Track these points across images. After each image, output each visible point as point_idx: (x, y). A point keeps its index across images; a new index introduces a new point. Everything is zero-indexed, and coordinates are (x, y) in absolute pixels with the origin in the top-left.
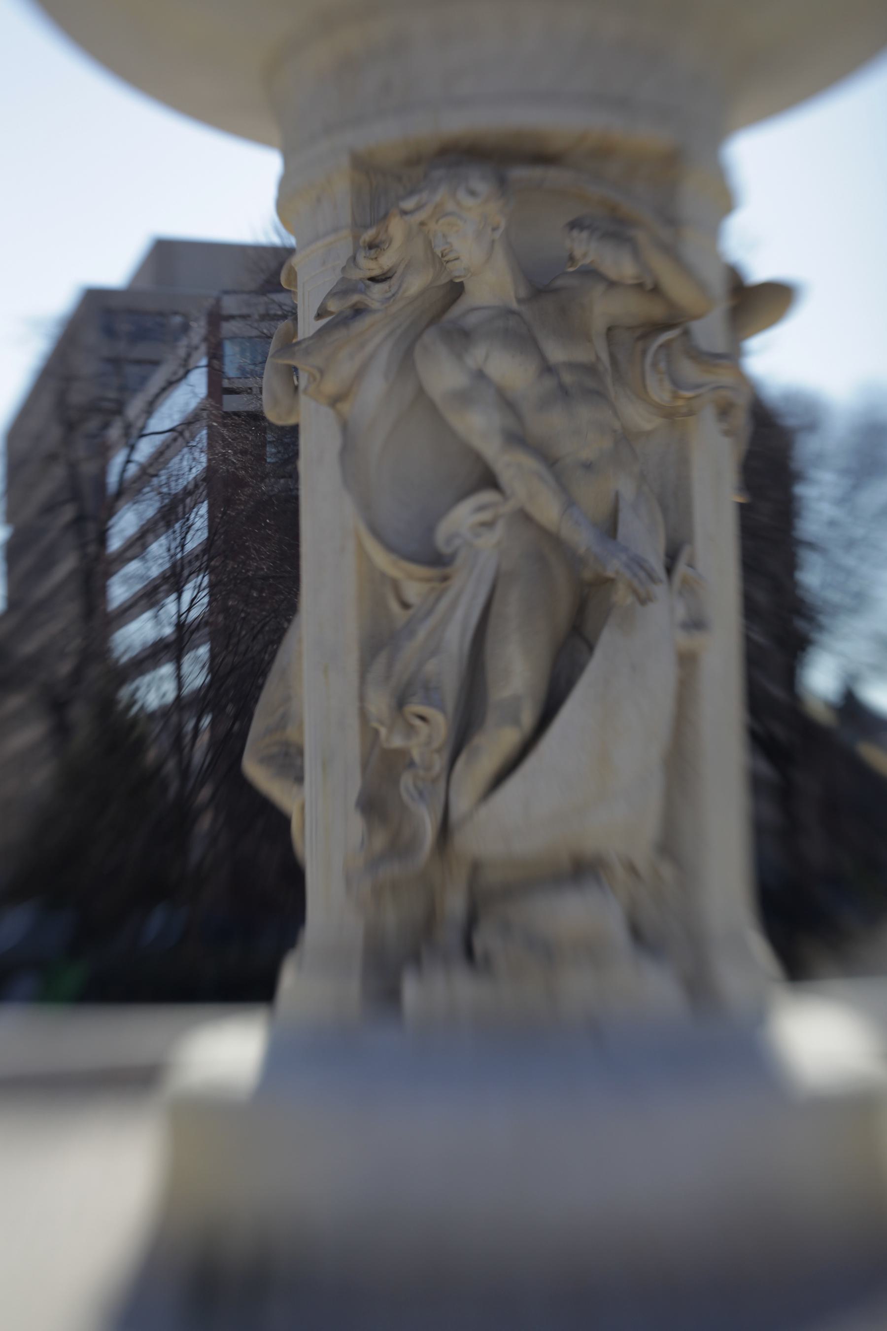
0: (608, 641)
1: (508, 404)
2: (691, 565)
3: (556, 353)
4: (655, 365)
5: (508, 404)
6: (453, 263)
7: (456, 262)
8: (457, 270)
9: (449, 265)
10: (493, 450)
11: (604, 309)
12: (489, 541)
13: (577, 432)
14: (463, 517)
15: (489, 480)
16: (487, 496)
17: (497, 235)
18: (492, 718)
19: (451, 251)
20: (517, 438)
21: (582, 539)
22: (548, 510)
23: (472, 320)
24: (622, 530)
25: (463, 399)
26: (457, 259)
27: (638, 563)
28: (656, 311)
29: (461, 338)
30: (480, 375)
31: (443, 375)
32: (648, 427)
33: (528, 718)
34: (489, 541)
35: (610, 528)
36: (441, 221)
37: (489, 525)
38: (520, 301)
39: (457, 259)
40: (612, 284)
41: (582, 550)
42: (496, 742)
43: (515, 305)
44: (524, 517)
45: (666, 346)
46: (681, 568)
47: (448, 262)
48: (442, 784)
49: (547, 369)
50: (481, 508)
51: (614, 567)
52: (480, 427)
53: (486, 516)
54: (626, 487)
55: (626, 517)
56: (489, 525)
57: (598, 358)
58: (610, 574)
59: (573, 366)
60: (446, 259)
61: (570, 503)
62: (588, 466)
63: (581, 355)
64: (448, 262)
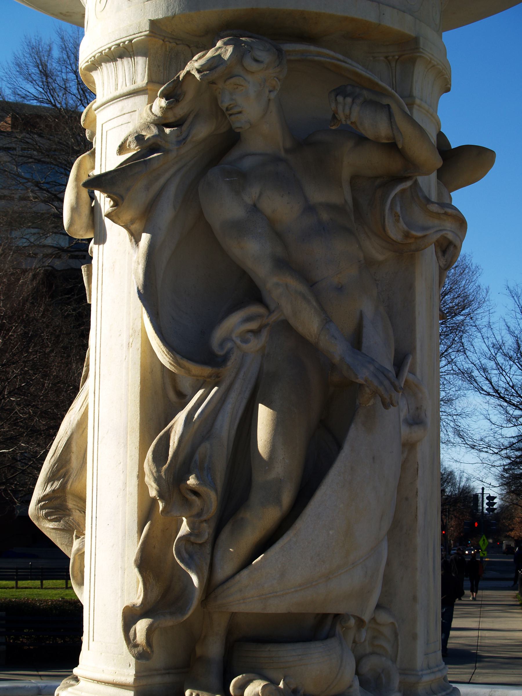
0: (355, 438)
1: (277, 233)
2: (412, 372)
3: (318, 195)
4: (391, 208)
5: (277, 233)
6: (237, 116)
7: (239, 116)
8: (239, 123)
9: (233, 118)
10: (263, 272)
11: (352, 161)
12: (254, 345)
13: (334, 259)
14: (234, 324)
15: (251, 293)
16: (255, 309)
17: (273, 96)
18: (256, 497)
19: (236, 106)
20: (283, 264)
21: (337, 349)
22: (310, 323)
23: (247, 163)
24: (366, 343)
25: (239, 228)
26: (240, 112)
27: (382, 370)
28: (395, 165)
29: (240, 179)
30: (255, 209)
31: (225, 207)
32: (381, 257)
33: (287, 498)
34: (254, 345)
35: (356, 341)
36: (228, 82)
37: (256, 333)
38: (287, 151)
39: (240, 112)
40: (361, 140)
41: (337, 359)
42: (261, 518)
43: (283, 154)
44: (285, 327)
45: (403, 191)
46: (406, 374)
47: (231, 115)
48: (208, 549)
49: (310, 209)
50: (249, 319)
51: (364, 375)
52: (253, 252)
53: (253, 325)
54: (368, 307)
55: (368, 330)
56: (256, 333)
57: (346, 201)
58: (361, 381)
59: (330, 207)
60: (230, 112)
61: (327, 320)
62: (340, 289)
63: (334, 198)
64: (231, 115)
